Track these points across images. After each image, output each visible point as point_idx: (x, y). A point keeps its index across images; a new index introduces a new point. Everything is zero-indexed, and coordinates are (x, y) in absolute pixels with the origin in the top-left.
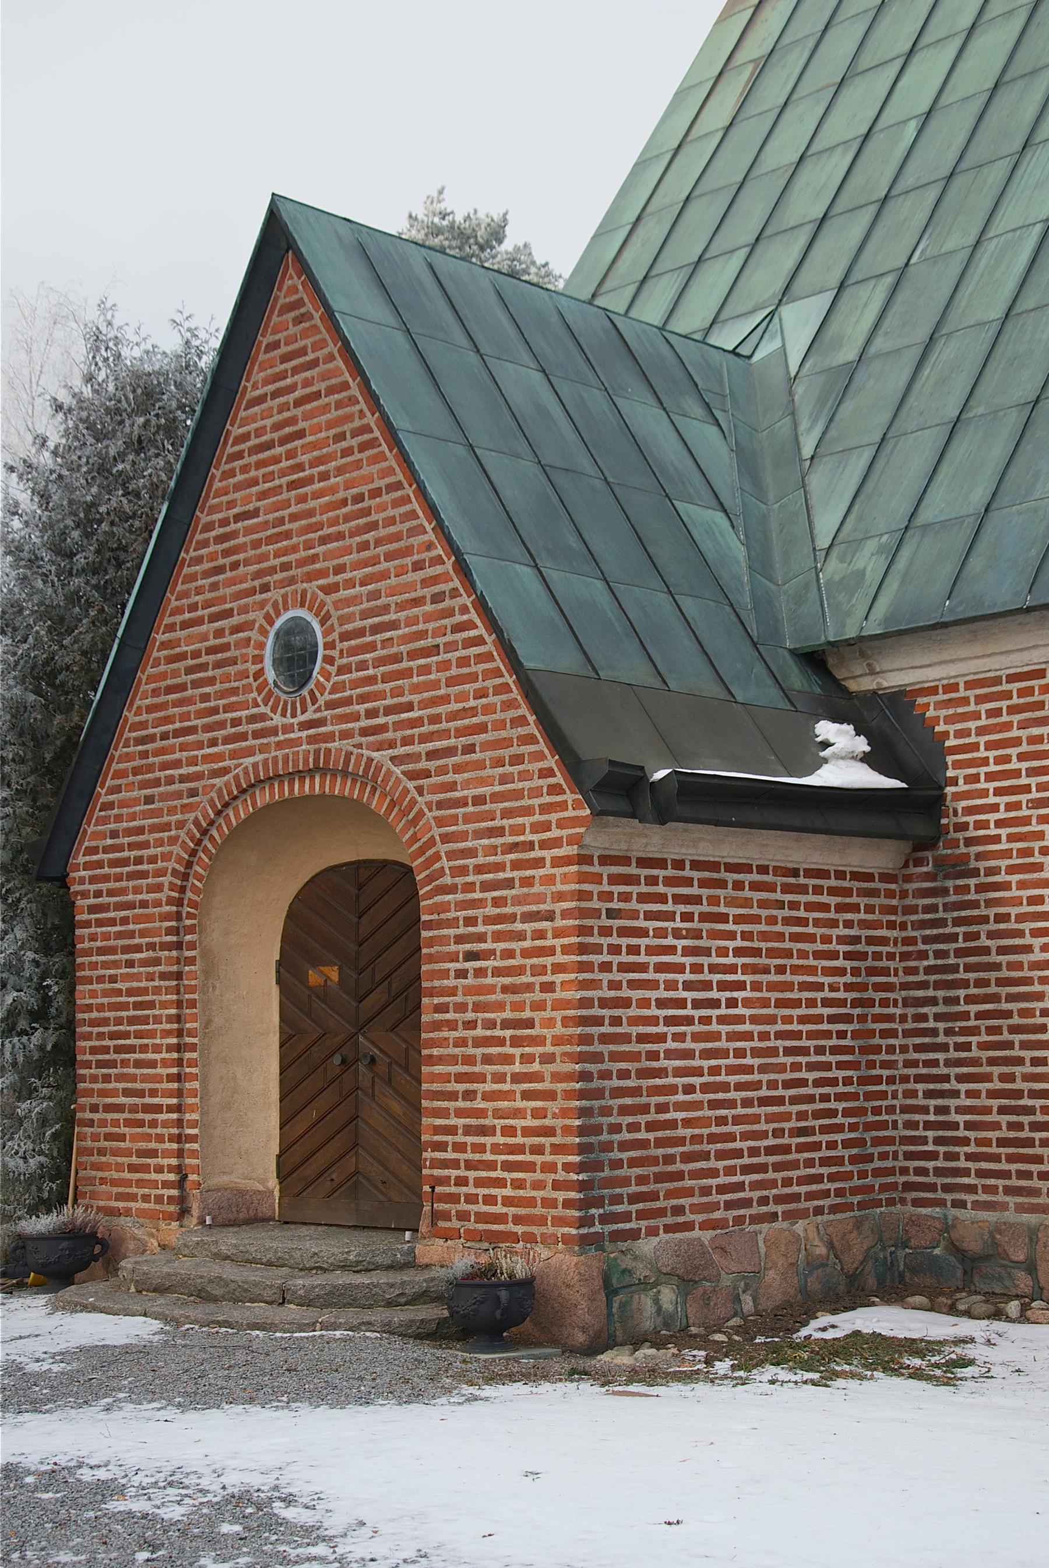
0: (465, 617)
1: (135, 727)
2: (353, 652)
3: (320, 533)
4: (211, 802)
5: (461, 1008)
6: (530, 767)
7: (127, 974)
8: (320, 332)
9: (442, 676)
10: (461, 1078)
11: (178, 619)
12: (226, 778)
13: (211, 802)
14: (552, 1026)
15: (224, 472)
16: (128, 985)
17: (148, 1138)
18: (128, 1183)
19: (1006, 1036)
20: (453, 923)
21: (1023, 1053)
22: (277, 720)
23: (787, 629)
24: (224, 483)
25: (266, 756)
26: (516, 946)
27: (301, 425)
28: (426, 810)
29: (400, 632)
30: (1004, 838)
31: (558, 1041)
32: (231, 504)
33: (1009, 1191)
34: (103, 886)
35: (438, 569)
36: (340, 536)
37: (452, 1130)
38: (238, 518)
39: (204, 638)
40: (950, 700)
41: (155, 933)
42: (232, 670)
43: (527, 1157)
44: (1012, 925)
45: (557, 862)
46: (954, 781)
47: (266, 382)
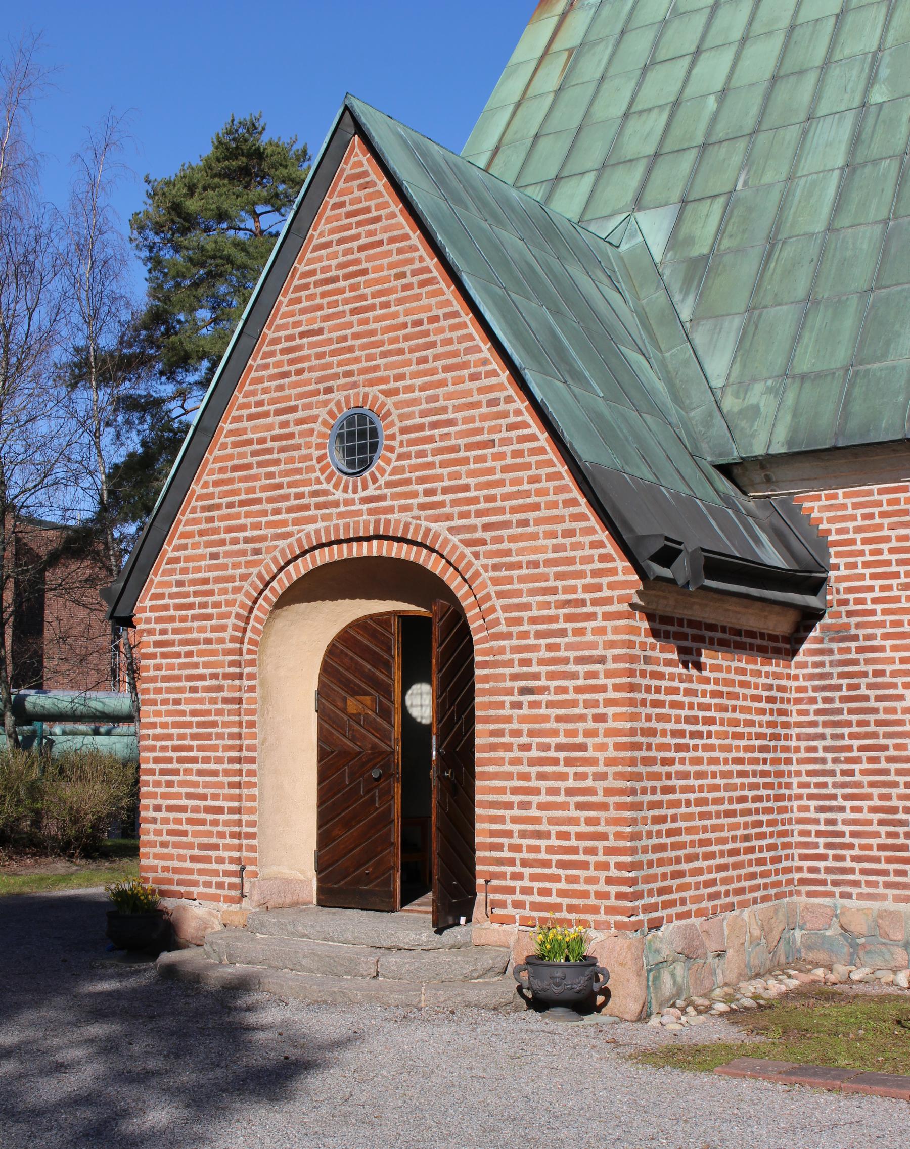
0: (519, 419)
1: (201, 498)
2: (412, 443)
3: (382, 349)
4: (275, 560)
5: (517, 733)
6: (582, 539)
7: (191, 698)
8: (383, 196)
9: (498, 464)
10: (515, 791)
11: (245, 412)
12: (289, 540)
13: (275, 560)
14: (603, 749)
15: (290, 300)
16: (192, 707)
17: (209, 834)
18: (190, 871)
19: (883, 765)
20: (509, 663)
21: (897, 778)
22: (339, 495)
23: (704, 446)
24: (291, 308)
25: (327, 523)
26: (570, 684)
27: (364, 265)
28: (482, 571)
29: (457, 428)
30: (879, 612)
31: (610, 762)
32: (297, 324)
33: (887, 885)
34: (169, 626)
35: (493, 380)
36: (401, 352)
37: (508, 834)
38: (302, 335)
39: (270, 427)
40: (831, 505)
41: (220, 665)
42: (296, 454)
43: (581, 857)
44: (887, 679)
45: (607, 616)
46: (836, 567)
47: (332, 232)
